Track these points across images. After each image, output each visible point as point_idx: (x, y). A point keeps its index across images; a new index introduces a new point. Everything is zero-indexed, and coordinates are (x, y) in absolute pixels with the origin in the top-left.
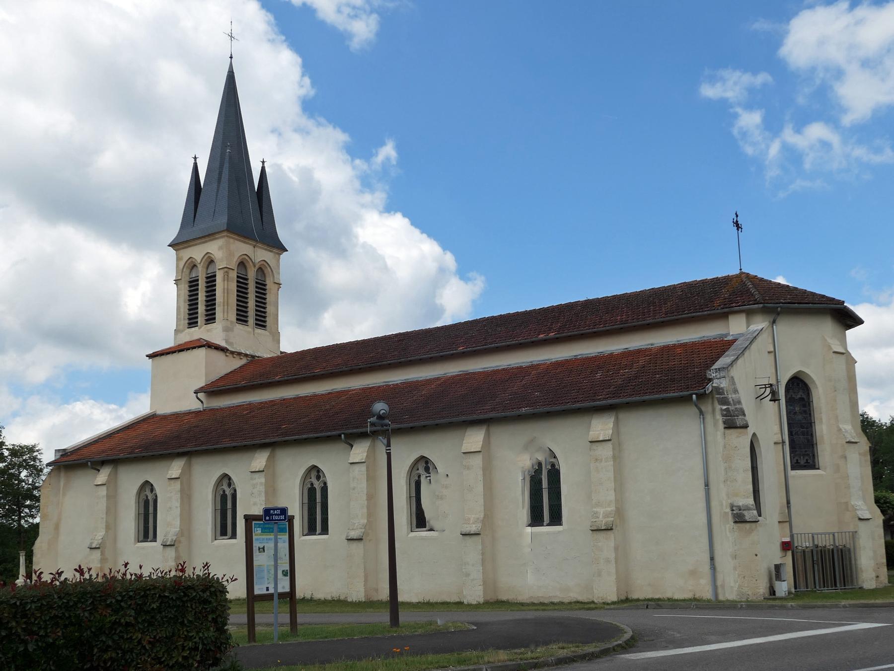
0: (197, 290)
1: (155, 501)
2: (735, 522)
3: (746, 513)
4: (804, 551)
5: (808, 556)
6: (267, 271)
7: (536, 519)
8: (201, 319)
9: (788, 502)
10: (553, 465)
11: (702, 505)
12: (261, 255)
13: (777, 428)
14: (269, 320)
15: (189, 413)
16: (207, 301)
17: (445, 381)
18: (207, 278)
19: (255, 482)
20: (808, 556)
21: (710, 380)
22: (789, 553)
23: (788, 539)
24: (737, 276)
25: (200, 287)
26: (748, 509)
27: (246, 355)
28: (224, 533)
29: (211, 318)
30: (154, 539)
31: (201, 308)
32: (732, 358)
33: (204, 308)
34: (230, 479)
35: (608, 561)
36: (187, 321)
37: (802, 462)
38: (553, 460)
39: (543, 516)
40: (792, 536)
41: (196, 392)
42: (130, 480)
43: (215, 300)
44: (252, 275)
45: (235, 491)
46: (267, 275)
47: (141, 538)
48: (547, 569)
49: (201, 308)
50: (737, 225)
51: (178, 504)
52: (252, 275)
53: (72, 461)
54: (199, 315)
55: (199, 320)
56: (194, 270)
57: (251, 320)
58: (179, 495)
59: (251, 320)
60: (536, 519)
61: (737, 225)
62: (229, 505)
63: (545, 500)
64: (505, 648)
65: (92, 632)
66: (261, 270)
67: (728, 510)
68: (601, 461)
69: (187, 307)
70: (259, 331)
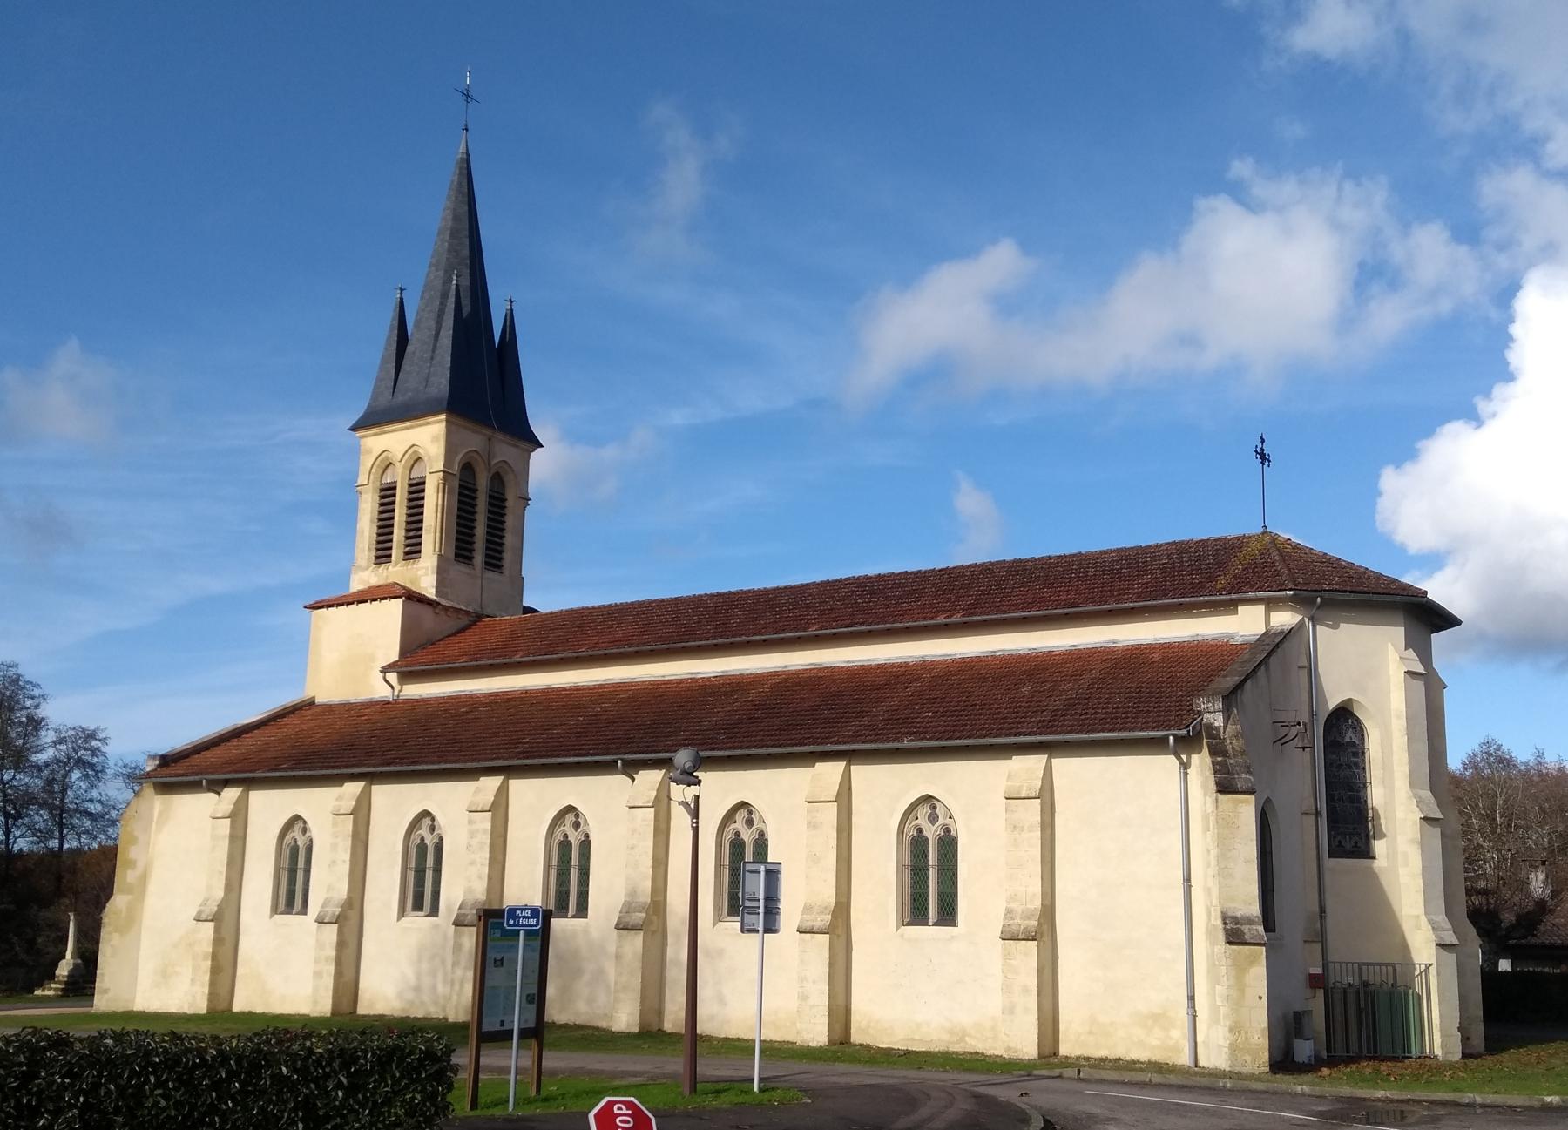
0: (393, 503)
1: (309, 849)
2: (1230, 943)
3: (1246, 929)
4: (1345, 991)
5: (1351, 998)
6: (509, 479)
7: (916, 912)
8: (397, 552)
9: (1322, 910)
10: (947, 830)
11: (1180, 909)
12: (504, 450)
13: (1307, 790)
14: (507, 556)
15: (371, 704)
16: (408, 523)
17: (775, 686)
18: (411, 485)
19: (474, 827)
20: (1351, 998)
21: (1199, 713)
22: (1320, 993)
23: (1319, 971)
24: (1259, 537)
25: (398, 499)
26: (1249, 921)
27: (468, 613)
28: (418, 906)
29: (413, 551)
30: (304, 911)
31: (398, 534)
32: (1237, 679)
33: (403, 533)
34: (433, 819)
35: (1026, 990)
36: (374, 553)
37: (1348, 846)
38: (948, 821)
39: (927, 909)
40: (1325, 966)
41: (384, 670)
42: (271, 808)
43: (421, 521)
44: (483, 483)
45: (441, 839)
46: (508, 485)
47: (282, 906)
48: (939, 996)
49: (398, 534)
50: (1263, 457)
51: (347, 857)
52: (483, 483)
53: (179, 771)
54: (395, 544)
55: (394, 552)
56: (389, 470)
57: (479, 558)
58: (349, 843)
59: (479, 558)
60: (916, 912)
61: (1263, 457)
62: (430, 862)
63: (930, 886)
64: (1296, 1094)
65: (62, 839)
66: (498, 480)
67: (1219, 922)
68: (1022, 829)
69: (375, 530)
70: (491, 575)
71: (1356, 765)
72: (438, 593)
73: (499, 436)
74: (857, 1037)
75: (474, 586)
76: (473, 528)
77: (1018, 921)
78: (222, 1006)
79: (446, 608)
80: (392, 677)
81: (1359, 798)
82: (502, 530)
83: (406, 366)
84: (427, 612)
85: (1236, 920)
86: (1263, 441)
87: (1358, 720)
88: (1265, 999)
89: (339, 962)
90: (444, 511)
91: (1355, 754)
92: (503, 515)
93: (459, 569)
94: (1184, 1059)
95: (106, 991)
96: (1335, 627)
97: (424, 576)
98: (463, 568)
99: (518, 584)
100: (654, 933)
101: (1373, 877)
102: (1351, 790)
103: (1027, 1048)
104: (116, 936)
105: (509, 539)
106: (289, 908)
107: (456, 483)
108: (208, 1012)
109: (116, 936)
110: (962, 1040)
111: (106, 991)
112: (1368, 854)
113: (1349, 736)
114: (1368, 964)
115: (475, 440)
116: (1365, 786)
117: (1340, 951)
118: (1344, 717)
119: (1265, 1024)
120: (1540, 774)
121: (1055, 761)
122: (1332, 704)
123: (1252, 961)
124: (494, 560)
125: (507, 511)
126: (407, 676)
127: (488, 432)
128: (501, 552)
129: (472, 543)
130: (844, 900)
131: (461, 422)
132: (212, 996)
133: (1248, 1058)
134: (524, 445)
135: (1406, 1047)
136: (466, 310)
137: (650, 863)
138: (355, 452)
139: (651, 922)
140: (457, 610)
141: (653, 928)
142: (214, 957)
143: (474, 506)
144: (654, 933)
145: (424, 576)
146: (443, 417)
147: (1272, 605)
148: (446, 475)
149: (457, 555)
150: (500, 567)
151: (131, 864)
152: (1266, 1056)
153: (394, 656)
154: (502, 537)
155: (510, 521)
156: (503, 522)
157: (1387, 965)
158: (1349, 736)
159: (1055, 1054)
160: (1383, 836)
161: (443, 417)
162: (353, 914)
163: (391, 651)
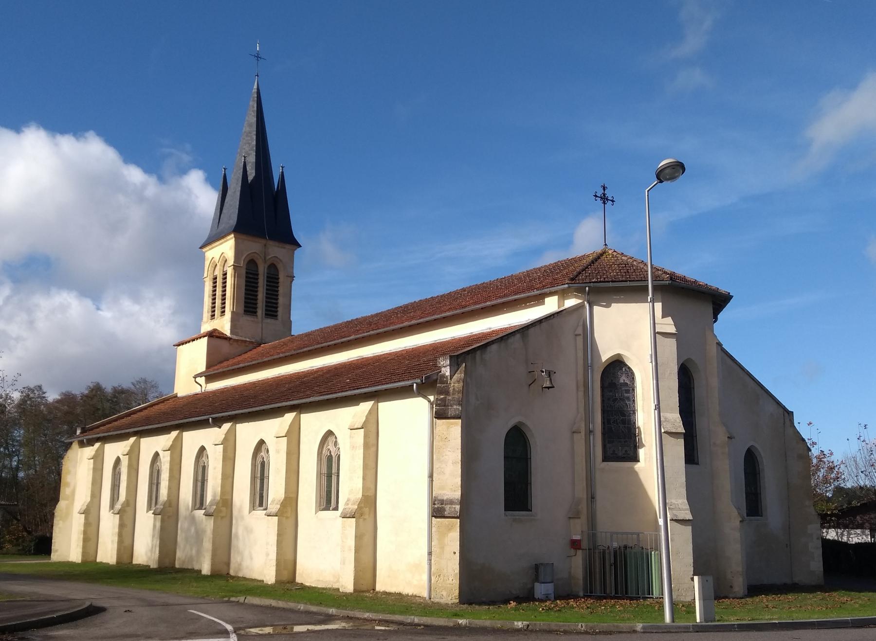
3: (447, 507)
4: (604, 551)
12: (276, 250)
14: (280, 310)
20: (610, 560)
27: (252, 343)
44: (262, 269)
47: (198, 506)
50: (604, 199)
52: (262, 269)
57: (260, 312)
59: (260, 312)
71: (628, 398)
72: (232, 332)
73: (271, 243)
74: (298, 580)
75: (253, 327)
76: (257, 296)
77: (350, 506)
78: (91, 559)
79: (237, 341)
80: (201, 380)
81: (630, 420)
82: (277, 295)
83: (224, 211)
84: (225, 345)
85: (442, 502)
86: (604, 188)
87: (629, 368)
88: (458, 554)
89: (120, 535)
90: (236, 287)
91: (628, 391)
92: (278, 287)
93: (247, 320)
94: (425, 594)
95: (57, 551)
96: (608, 306)
97: (224, 325)
98: (249, 318)
99: (288, 324)
100: (222, 518)
101: (635, 474)
102: (624, 415)
103: (347, 585)
104: (61, 522)
105: (281, 300)
106: (327, 508)
107: (244, 271)
108: (118, 563)
109: (61, 522)
110: (338, 581)
111: (57, 551)
112: (636, 459)
113: (623, 379)
114: (617, 533)
115: (255, 246)
116: (634, 413)
117: (604, 525)
118: (617, 364)
119: (457, 571)
120: (92, 390)
121: (380, 404)
122: (606, 355)
123: (450, 528)
124: (272, 311)
125: (280, 284)
126: (210, 377)
127: (263, 241)
128: (277, 308)
129: (256, 304)
130: (293, 495)
131: (244, 237)
132: (84, 553)
133: (444, 593)
134: (288, 246)
135: (650, 591)
136: (251, 174)
137: (220, 477)
138: (203, 258)
139: (221, 511)
140: (246, 341)
141: (223, 514)
142: (85, 533)
143: (257, 283)
144: (222, 518)
145: (224, 325)
146: (232, 235)
147: (563, 295)
148: (236, 267)
149: (245, 311)
150: (276, 316)
151: (68, 485)
152: (457, 592)
153: (202, 368)
154: (277, 299)
155: (281, 290)
156: (277, 291)
157: (634, 533)
158: (623, 379)
159: (374, 590)
160: (643, 446)
161: (232, 235)
162: (129, 510)
163: (201, 366)
